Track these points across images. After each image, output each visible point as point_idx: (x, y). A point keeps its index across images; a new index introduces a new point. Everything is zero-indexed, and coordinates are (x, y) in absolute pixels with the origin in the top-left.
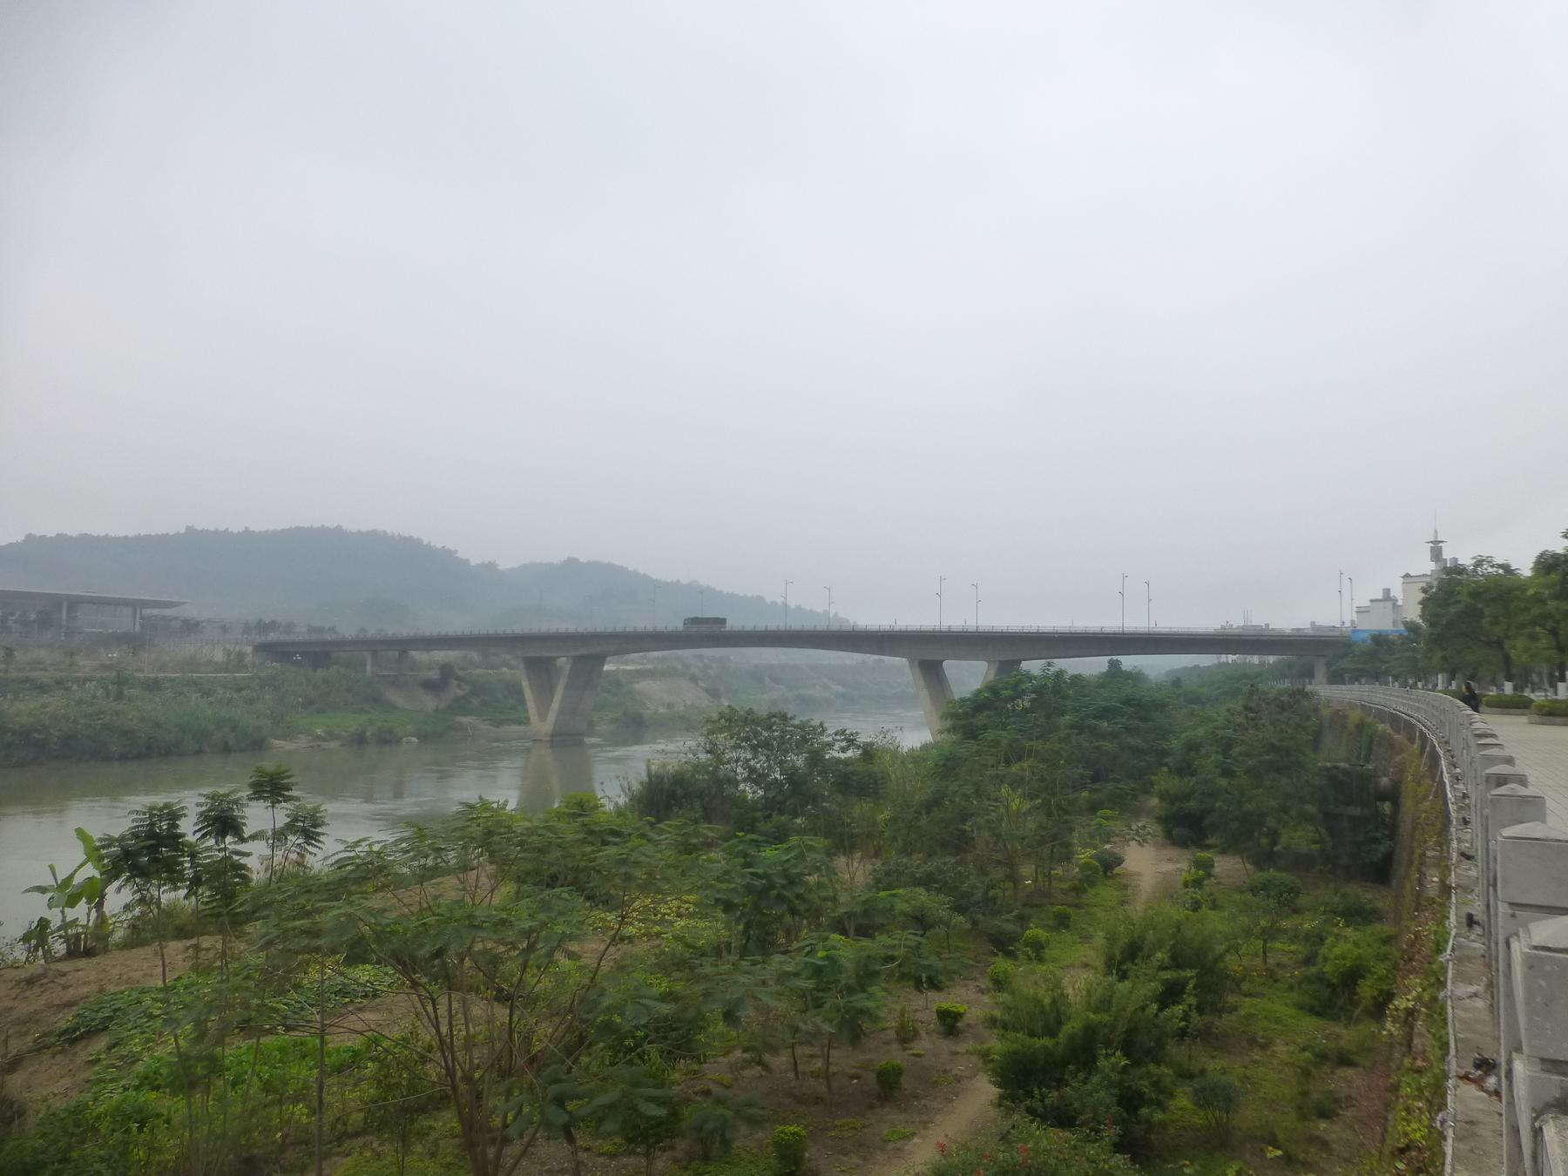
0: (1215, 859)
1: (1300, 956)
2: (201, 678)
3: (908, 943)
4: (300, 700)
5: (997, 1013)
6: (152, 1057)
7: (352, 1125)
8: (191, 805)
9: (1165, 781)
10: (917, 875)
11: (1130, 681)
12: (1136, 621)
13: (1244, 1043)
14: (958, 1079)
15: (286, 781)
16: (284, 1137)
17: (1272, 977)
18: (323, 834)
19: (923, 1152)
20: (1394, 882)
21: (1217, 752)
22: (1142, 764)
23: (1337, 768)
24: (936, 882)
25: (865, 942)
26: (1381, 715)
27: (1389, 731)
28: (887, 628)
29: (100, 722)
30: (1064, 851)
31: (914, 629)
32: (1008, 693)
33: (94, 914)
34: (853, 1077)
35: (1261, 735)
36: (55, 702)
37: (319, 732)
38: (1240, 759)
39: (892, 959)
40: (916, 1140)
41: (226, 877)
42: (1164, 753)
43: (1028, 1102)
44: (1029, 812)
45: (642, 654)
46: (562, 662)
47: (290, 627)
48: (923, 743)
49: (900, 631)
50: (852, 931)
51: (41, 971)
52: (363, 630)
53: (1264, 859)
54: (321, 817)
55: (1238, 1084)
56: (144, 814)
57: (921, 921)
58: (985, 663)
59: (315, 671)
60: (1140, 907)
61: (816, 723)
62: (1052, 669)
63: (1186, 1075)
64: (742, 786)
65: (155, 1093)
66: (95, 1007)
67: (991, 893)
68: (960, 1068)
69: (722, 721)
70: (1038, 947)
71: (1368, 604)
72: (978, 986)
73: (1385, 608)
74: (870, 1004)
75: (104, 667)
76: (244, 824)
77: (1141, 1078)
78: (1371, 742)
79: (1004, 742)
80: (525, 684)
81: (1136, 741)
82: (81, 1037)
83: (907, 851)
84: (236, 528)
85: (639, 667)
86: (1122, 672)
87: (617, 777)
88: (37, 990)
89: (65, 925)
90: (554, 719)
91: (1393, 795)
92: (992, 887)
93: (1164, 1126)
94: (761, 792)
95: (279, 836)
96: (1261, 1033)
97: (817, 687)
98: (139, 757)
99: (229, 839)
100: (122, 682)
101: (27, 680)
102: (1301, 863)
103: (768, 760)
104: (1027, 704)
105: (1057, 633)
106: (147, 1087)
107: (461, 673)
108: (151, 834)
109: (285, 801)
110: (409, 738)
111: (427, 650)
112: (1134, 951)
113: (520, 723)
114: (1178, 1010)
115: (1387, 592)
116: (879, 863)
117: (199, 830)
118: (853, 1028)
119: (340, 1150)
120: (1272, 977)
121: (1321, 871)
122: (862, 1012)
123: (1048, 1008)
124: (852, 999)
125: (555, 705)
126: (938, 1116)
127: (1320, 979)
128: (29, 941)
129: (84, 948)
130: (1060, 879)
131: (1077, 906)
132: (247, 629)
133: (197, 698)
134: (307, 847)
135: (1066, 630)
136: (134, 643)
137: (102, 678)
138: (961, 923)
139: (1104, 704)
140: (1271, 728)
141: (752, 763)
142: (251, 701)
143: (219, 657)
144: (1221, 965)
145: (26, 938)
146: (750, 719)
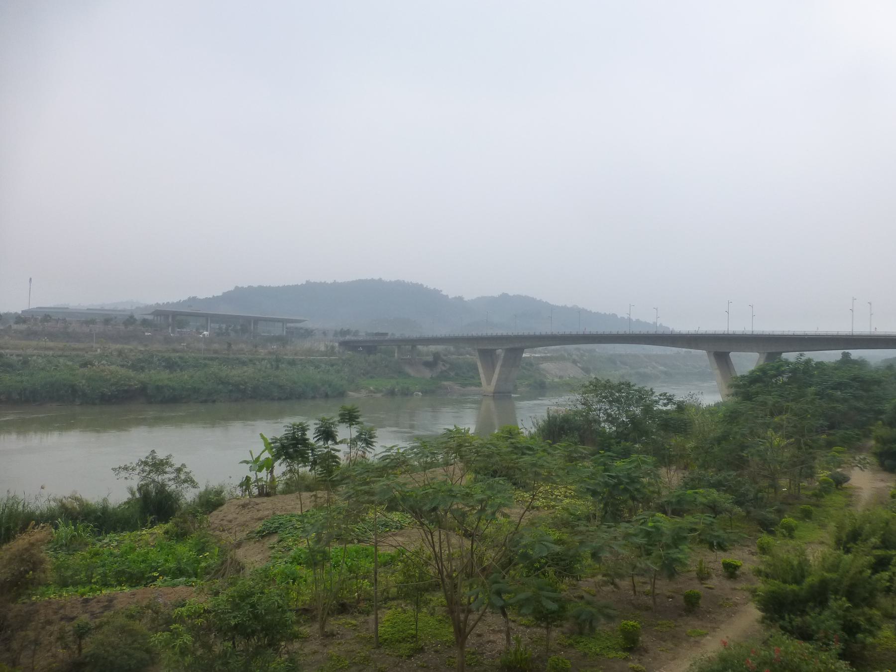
3: (705, 521)
6: (297, 548)
12: (862, 328)
14: (736, 605)
16: (359, 596)
18: (375, 442)
22: (864, 419)
24: (724, 486)
29: (269, 381)
32: (773, 372)
34: (669, 597)
36: (249, 370)
37: (372, 388)
39: (695, 530)
40: (708, 637)
42: (881, 412)
44: (786, 446)
46: (499, 351)
47: (356, 333)
48: (716, 402)
49: (770, 335)
51: (248, 501)
56: (290, 427)
57: (713, 509)
62: (803, 358)
64: (603, 425)
67: (760, 495)
72: (750, 550)
75: (270, 353)
76: (337, 435)
77: (858, 615)
80: (479, 364)
81: (860, 404)
84: (330, 281)
85: (543, 355)
88: (246, 510)
89: (257, 480)
92: (760, 491)
93: (874, 647)
94: (614, 428)
98: (287, 399)
99: (330, 442)
100: (278, 360)
101: (238, 359)
103: (619, 409)
107: (444, 358)
108: (294, 438)
109: (356, 424)
112: (855, 536)
114: (886, 575)
116: (687, 473)
117: (316, 437)
118: (670, 569)
122: (675, 560)
123: (796, 567)
125: (496, 376)
129: (266, 492)
130: (805, 488)
131: (817, 506)
132: (336, 334)
135: (813, 333)
136: (282, 340)
138: (740, 512)
141: (609, 411)
142: (338, 372)
143: (323, 348)
145: (241, 485)
146: (608, 386)
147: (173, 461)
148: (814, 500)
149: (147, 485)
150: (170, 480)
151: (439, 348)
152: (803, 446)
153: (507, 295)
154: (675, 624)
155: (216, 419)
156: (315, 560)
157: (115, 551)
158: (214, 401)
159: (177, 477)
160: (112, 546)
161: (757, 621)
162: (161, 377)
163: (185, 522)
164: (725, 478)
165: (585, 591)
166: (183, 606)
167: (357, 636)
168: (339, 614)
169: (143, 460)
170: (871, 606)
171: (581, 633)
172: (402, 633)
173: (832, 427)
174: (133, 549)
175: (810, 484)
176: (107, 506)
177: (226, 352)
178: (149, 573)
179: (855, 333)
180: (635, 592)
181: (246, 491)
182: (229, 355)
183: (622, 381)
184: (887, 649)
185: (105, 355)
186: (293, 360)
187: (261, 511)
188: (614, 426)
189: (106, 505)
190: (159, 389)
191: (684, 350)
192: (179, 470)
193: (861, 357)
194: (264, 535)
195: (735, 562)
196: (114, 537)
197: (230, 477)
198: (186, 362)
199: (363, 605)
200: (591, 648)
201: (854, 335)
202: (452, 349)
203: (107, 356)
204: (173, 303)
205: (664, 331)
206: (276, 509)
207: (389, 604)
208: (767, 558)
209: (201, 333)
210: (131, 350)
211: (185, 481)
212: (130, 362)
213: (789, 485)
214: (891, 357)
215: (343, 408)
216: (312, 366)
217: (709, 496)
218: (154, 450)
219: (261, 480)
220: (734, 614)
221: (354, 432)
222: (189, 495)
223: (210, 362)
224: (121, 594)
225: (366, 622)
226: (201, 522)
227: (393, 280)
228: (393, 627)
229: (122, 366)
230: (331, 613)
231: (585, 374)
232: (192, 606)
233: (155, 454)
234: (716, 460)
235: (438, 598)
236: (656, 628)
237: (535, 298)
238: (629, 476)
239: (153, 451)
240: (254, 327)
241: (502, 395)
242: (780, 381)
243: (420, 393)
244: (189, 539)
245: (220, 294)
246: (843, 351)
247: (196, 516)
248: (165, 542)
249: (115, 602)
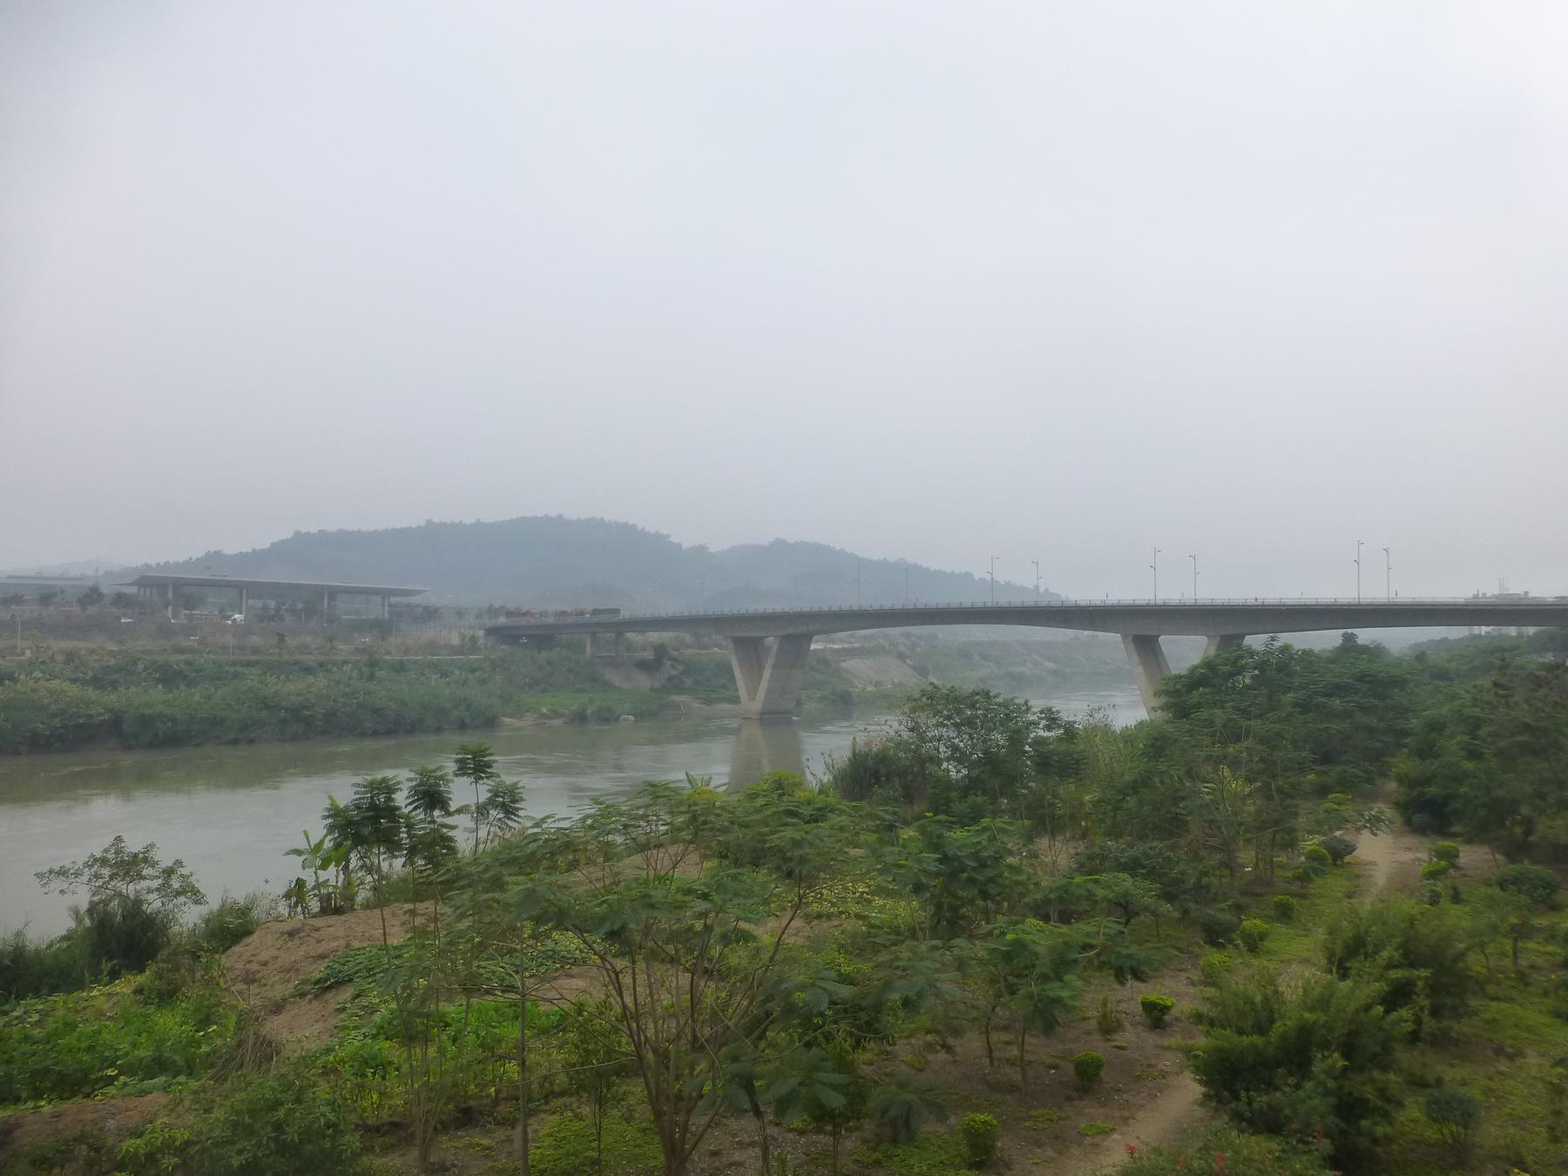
0: (1460, 849)
1: (1558, 957)
2: (439, 660)
3: (1107, 930)
4: (527, 680)
5: (1204, 1009)
6: (387, 1009)
7: (558, 1085)
8: (403, 779)
9: (1403, 763)
10: (1122, 860)
11: (1365, 656)
12: (1374, 592)
13: (1490, 1053)
14: (1164, 1075)
15: (487, 758)
16: (498, 1092)
17: (1523, 979)
18: (522, 809)
19: (1116, 1155)
22: (1378, 745)
24: (1144, 867)
25: (1065, 929)
28: (1099, 603)
29: (355, 701)
31: (1127, 603)
32: (1227, 668)
33: (341, 877)
36: (319, 682)
37: (544, 710)
38: (1489, 739)
39: (1092, 947)
40: (1116, 1136)
41: (436, 846)
42: (1405, 733)
43: (1233, 1105)
44: (1250, 795)
45: (851, 632)
46: (770, 641)
48: (1139, 721)
49: (1223, 605)
50: (1054, 916)
51: (299, 925)
53: (1517, 849)
54: (519, 793)
55: (1479, 1096)
56: (365, 787)
57: (1125, 908)
60: (1368, 900)
61: (1020, 701)
62: (1277, 644)
63: (1419, 1083)
64: (945, 765)
65: (388, 1042)
66: (342, 961)
67: (1205, 880)
68: (1168, 1062)
72: (1188, 978)
74: (1065, 994)
75: (359, 651)
76: (450, 799)
77: (1363, 1084)
79: (1219, 722)
80: (735, 664)
83: (1115, 833)
84: (469, 520)
88: (297, 942)
89: (318, 886)
92: (1206, 874)
93: (1389, 1139)
94: (964, 772)
95: (482, 810)
96: (1509, 1042)
98: (389, 733)
99: (436, 813)
100: (373, 664)
101: (296, 663)
103: (971, 738)
104: (1247, 681)
105: (1284, 605)
106: (384, 1036)
107: (675, 654)
108: (373, 806)
109: (487, 778)
110: (626, 716)
111: (642, 632)
114: (1404, 1013)
116: (1081, 847)
117: (410, 804)
118: (1046, 1017)
119: (547, 1108)
122: (1057, 1001)
123: (1259, 1006)
124: (1046, 987)
125: (764, 684)
126: (1140, 1113)
128: (290, 899)
129: (333, 907)
130: (1282, 866)
131: (1303, 896)
133: (436, 679)
134: (507, 821)
136: (382, 627)
137: (357, 661)
138: (1169, 911)
139: (1336, 680)
140: (1526, 707)
141: (957, 741)
142: (483, 682)
143: (455, 640)
144: (1461, 965)
145: (287, 896)
147: (156, 855)
148: (1295, 887)
149: (106, 902)
150: (150, 891)
151: (666, 636)
152: (1274, 794)
154: (1059, 1114)
156: (410, 1031)
157: (33, 1032)
158: (251, 741)
159: (166, 885)
160: (29, 1023)
161: (1195, 1102)
162: (151, 698)
163: (176, 969)
165: (905, 1062)
166: (140, 1135)
167: (490, 1168)
168: (458, 1129)
169: (98, 856)
170: (1385, 1068)
171: (895, 1141)
172: (574, 1158)
173: (1326, 759)
174: (71, 1026)
175: (1291, 858)
176: (24, 947)
177: (277, 651)
178: (99, 1071)
179: (1363, 601)
180: (991, 1057)
181: (296, 905)
185: (40, 660)
186: (401, 662)
187: (323, 943)
188: (965, 767)
189: (20, 944)
190: (145, 721)
192: (169, 872)
193: (1374, 641)
194: (325, 987)
195: (1162, 999)
197: (267, 882)
199: (504, 1109)
200: (913, 1165)
201: (1362, 603)
202: (688, 637)
203: (43, 663)
204: (177, 565)
205: (937, 604)
206: (351, 937)
207: (557, 1103)
208: (1211, 992)
209: (228, 618)
210: (92, 651)
212: (91, 673)
213: (1254, 862)
216: (436, 674)
217: (1117, 886)
218: (119, 837)
219: (325, 883)
220: (1159, 1092)
221: (483, 792)
223: (245, 670)
224: (32, 1117)
225: (510, 1140)
226: (207, 968)
228: (556, 1148)
229: (74, 681)
230: (444, 1127)
231: (921, 678)
232: (156, 1135)
233: (123, 845)
234: (1134, 821)
235: (636, 1089)
236: (1027, 1124)
237: (832, 546)
238: (976, 856)
239: (119, 839)
240: (329, 604)
242: (1239, 683)
243: (631, 718)
244: (182, 1001)
245: (264, 544)
247: (199, 957)
248: (134, 1009)
249: (17, 1133)
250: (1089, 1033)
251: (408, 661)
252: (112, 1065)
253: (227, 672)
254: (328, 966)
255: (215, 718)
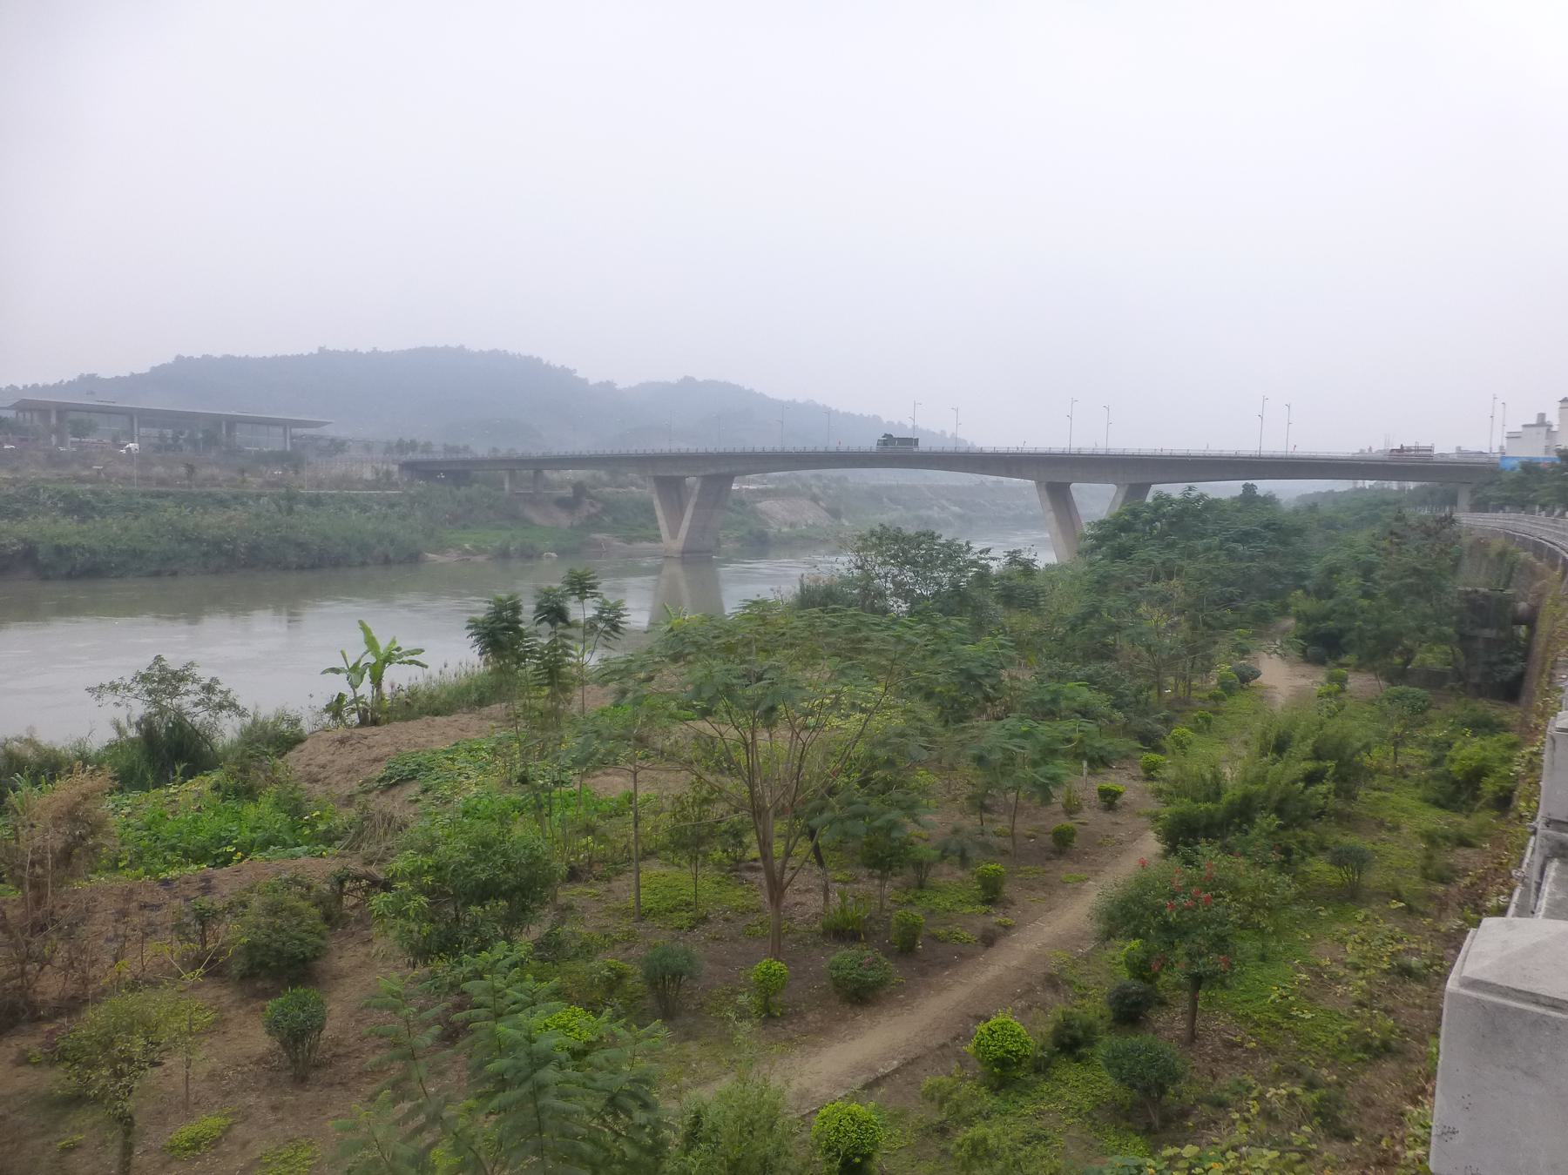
12: (1274, 445)
13: (1373, 826)
15: (591, 581)
20: (1524, 699)
21: (1357, 575)
23: (1476, 592)
26: (1524, 543)
27: (1532, 559)
30: (1206, 663)
34: (1030, 837)
35: (1404, 560)
37: (467, 546)
39: (1069, 741)
42: (1302, 576)
46: (690, 480)
47: (427, 447)
52: (495, 450)
53: (1398, 676)
57: (1085, 713)
58: (1114, 486)
59: (458, 489)
62: (1194, 494)
69: (874, 539)
70: (1182, 745)
71: (1520, 429)
73: (1538, 434)
77: (1289, 838)
78: (1512, 568)
80: (656, 502)
81: (1274, 565)
82: (396, 784)
85: (761, 487)
86: (1259, 496)
87: (772, 590)
88: (348, 748)
90: (684, 537)
91: (1530, 620)
96: (1389, 819)
97: (936, 508)
98: (313, 567)
100: (291, 498)
101: (209, 495)
102: (1433, 680)
107: (593, 492)
111: (557, 469)
112: (1281, 746)
113: (650, 540)
115: (1542, 416)
120: (1401, 773)
121: (1452, 689)
125: (686, 523)
127: (1447, 776)
131: (1216, 713)
132: (389, 449)
135: (1201, 453)
136: (292, 459)
142: (403, 517)
143: (368, 474)
145: (328, 709)
146: (898, 537)
153: (693, 379)
155: (289, 604)
158: (174, 574)
164: (1097, 672)
169: (144, 672)
182: (190, 487)
183: (922, 529)
184: (1319, 885)
191: (994, 478)
192: (209, 689)
196: (120, 800)
197: (311, 696)
198: (107, 502)
204: (46, 387)
209: (122, 446)
211: (221, 707)
214: (1311, 491)
215: (571, 572)
222: (228, 730)
227: (486, 348)
239: (158, 659)
241: (698, 557)
243: (553, 554)
245: (143, 368)
246: (1244, 482)
250: (1055, 814)
251: (325, 494)
252: (229, 843)
253: (138, 503)
254: (389, 767)
255: (134, 550)
